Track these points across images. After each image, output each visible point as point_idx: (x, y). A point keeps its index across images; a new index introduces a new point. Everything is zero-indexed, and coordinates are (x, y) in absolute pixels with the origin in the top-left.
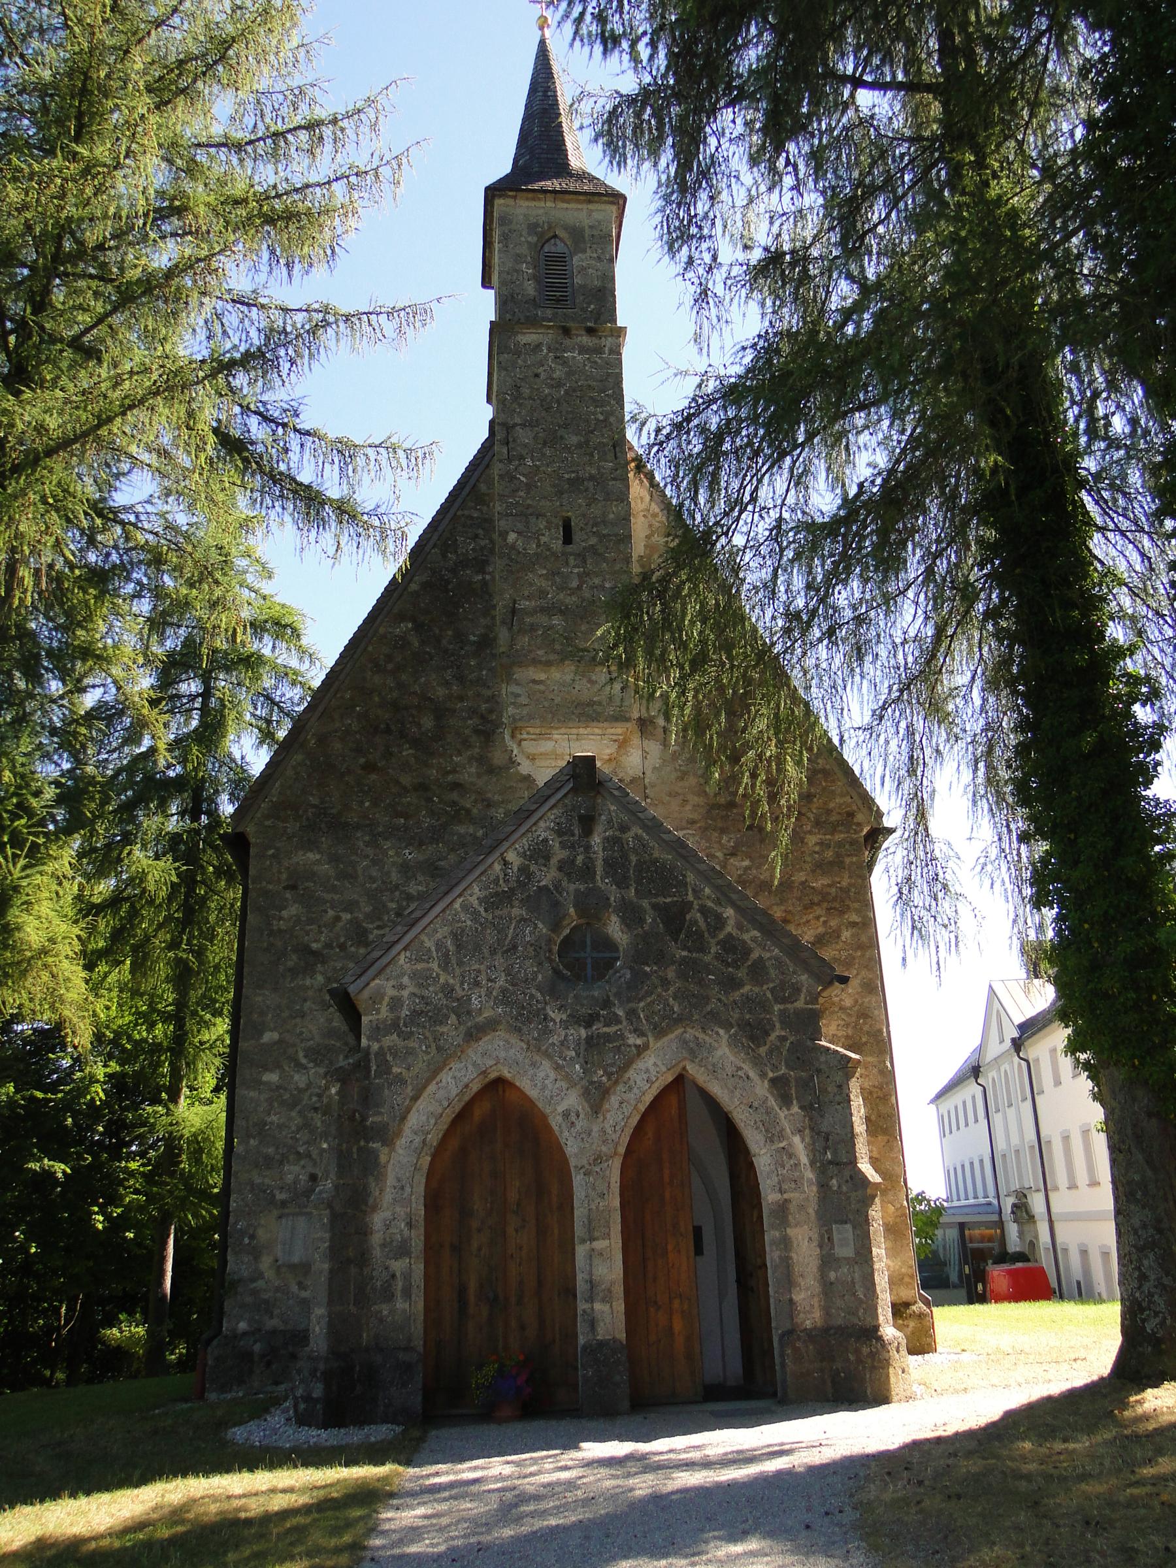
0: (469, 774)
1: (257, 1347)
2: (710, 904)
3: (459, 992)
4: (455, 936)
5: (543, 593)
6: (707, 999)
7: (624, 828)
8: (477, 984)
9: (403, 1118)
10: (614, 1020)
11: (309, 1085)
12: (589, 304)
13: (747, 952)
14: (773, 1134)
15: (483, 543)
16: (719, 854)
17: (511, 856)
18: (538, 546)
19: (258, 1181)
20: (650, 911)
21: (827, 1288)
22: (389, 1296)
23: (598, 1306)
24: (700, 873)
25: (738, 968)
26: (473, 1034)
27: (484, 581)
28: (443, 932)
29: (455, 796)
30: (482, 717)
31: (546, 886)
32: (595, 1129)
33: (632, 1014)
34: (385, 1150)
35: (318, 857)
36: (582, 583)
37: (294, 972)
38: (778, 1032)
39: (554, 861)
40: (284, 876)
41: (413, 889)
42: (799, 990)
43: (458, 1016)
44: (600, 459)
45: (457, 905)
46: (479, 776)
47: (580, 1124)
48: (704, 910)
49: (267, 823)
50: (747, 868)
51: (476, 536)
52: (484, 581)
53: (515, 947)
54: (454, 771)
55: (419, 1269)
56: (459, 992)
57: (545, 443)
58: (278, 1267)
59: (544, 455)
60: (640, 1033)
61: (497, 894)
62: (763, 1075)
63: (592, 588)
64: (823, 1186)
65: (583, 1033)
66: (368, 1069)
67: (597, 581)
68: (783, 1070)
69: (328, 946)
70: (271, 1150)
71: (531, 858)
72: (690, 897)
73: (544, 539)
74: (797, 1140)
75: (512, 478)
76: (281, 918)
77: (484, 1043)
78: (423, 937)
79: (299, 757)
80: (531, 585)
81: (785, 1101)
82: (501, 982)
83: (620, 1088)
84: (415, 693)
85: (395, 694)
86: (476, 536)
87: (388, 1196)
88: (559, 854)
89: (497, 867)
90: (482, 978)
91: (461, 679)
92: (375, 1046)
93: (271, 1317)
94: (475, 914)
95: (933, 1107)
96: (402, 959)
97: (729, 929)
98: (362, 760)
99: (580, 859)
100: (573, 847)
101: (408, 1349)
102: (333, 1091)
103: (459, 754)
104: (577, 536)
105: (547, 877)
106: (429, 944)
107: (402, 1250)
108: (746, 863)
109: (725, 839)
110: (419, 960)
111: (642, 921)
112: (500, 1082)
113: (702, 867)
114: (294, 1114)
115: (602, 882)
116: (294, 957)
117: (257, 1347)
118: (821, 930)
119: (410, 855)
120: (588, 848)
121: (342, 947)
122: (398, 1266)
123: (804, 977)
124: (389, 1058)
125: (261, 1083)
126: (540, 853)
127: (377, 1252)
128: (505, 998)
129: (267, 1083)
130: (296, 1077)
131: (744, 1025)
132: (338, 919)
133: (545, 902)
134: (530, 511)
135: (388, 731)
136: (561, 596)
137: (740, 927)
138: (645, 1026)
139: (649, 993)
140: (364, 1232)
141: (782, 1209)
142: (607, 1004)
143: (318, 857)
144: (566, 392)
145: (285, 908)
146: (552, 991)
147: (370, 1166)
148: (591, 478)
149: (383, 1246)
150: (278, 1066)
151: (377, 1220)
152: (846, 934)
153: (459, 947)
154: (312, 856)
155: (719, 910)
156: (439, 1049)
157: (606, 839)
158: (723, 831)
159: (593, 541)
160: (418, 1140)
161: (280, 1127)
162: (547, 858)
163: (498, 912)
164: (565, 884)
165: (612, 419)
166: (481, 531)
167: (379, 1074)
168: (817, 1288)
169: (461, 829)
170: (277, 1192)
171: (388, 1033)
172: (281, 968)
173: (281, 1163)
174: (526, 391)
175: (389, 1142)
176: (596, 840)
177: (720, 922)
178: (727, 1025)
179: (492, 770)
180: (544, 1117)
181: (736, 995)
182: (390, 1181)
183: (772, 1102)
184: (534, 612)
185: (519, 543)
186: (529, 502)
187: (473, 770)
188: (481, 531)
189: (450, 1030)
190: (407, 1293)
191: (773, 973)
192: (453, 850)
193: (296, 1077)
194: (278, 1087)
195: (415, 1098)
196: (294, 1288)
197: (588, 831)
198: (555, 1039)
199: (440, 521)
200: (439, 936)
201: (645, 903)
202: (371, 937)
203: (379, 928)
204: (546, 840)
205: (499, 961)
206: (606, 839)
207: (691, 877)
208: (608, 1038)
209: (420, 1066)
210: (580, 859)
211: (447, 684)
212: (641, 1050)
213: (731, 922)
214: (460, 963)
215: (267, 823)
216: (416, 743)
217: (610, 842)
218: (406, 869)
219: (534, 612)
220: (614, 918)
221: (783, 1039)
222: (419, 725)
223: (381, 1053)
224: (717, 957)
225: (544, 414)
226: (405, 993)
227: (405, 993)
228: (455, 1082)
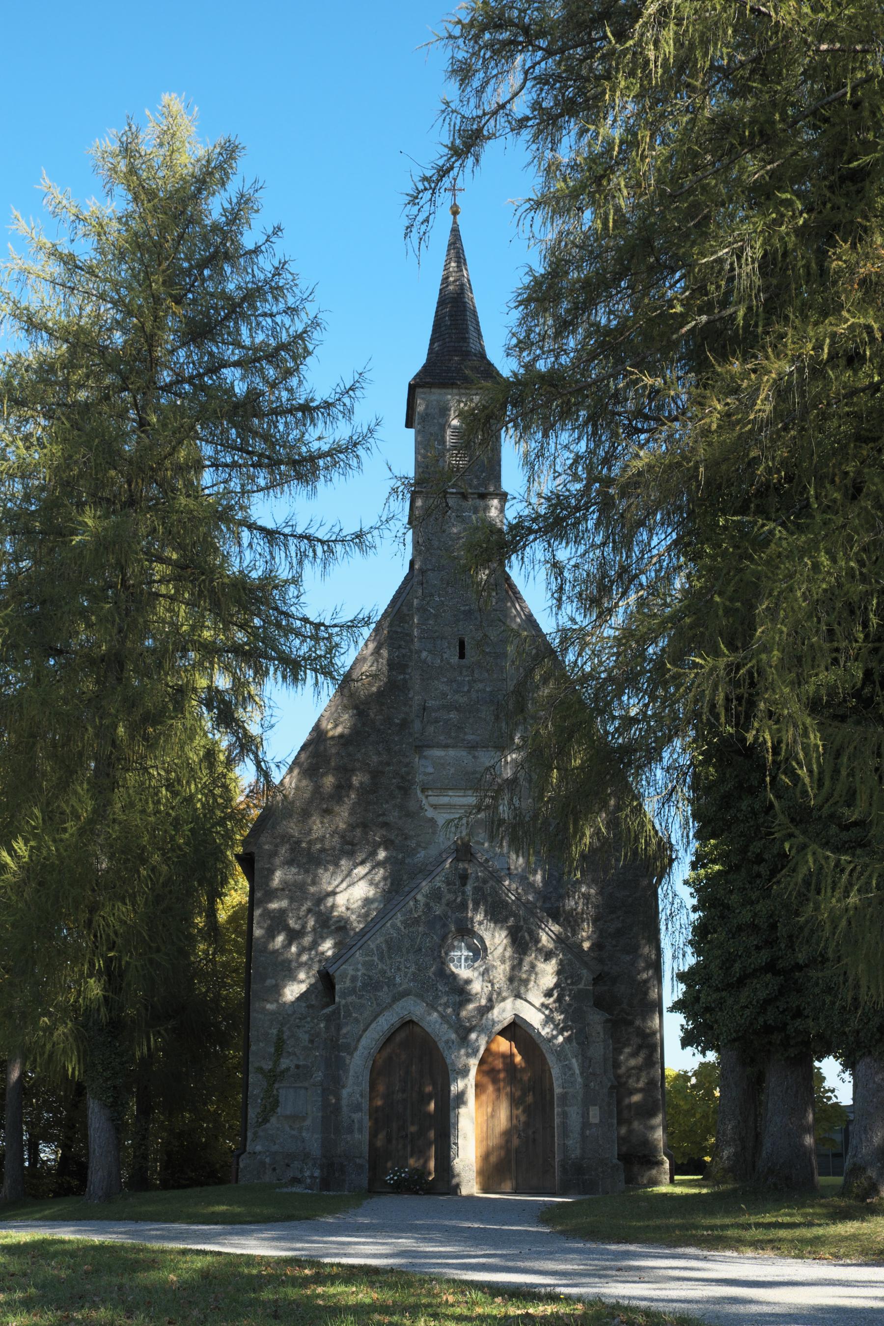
1: (268, 1160)
3: (389, 974)
5: (444, 695)
7: (485, 882)
8: (399, 969)
9: (359, 1040)
15: (404, 651)
17: (419, 897)
18: (442, 661)
21: (584, 1137)
22: (350, 1131)
26: (397, 998)
27: (404, 679)
28: (380, 940)
30: (402, 777)
34: (348, 1057)
39: (444, 901)
42: (581, 979)
45: (388, 925)
46: (400, 818)
51: (400, 647)
52: (404, 679)
53: (420, 949)
54: (384, 814)
56: (389, 974)
63: (477, 691)
64: (586, 1086)
66: (339, 1013)
67: (480, 686)
72: (522, 923)
74: (574, 1061)
77: (401, 1003)
78: (369, 942)
86: (400, 647)
87: (351, 1081)
89: (411, 903)
90: (402, 967)
92: (343, 1002)
99: (459, 900)
102: (322, 1025)
103: (387, 802)
106: (372, 946)
107: (357, 1108)
112: (411, 1022)
120: (464, 893)
122: (356, 1116)
123: (585, 971)
136: (456, 697)
149: (348, 1106)
153: (389, 948)
156: (378, 1005)
157: (475, 888)
160: (366, 1052)
162: (440, 899)
166: (403, 643)
167: (345, 1017)
174: (436, 543)
175: (351, 1054)
179: (409, 815)
180: (435, 1042)
182: (351, 1073)
187: (396, 814)
188: (403, 643)
189: (384, 995)
190: (360, 1130)
195: (365, 1030)
197: (464, 884)
206: (475, 888)
210: (459, 900)
226: (359, 973)
228: (386, 1022)
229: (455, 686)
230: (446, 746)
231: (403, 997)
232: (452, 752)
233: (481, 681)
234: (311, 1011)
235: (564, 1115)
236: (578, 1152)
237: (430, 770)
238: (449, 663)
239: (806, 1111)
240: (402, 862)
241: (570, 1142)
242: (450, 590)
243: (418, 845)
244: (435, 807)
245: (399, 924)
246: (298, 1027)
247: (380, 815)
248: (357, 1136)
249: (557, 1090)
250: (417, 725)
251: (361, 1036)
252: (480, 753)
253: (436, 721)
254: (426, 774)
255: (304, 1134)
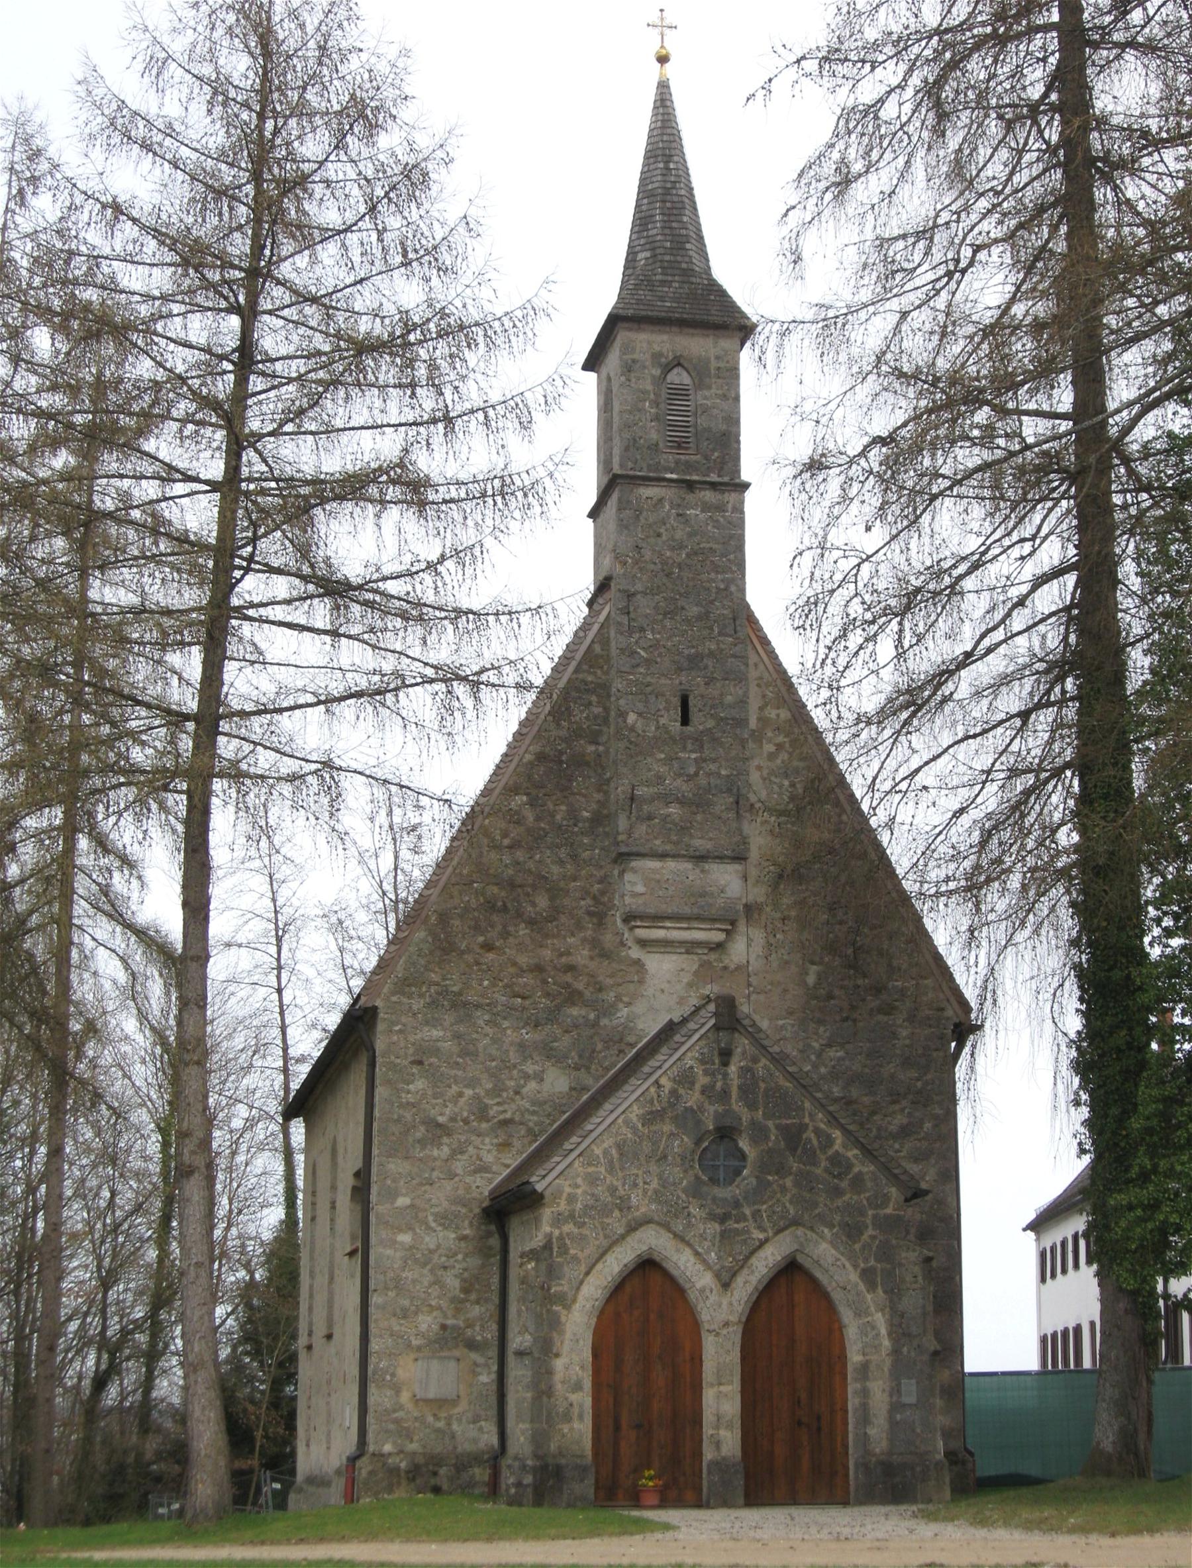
1: (403, 1465)
2: (822, 1126)
4: (618, 1146)
5: (660, 779)
6: (816, 1205)
7: (755, 1060)
8: (635, 1185)
9: (578, 1289)
10: (742, 1218)
11: (439, 1246)
12: (713, 450)
13: (850, 1166)
16: (816, 1045)
17: (663, 1081)
18: (658, 728)
19: (396, 1328)
20: (774, 1130)
21: (893, 1424)
23: (722, 1432)
25: (841, 1179)
26: (632, 1228)
28: (608, 1142)
29: (568, 978)
31: (691, 1108)
32: (725, 1302)
33: (756, 1214)
34: (564, 1312)
35: (441, 1034)
36: (699, 768)
37: (423, 1143)
38: (870, 1231)
39: (698, 1087)
40: (411, 1051)
41: (530, 1068)
42: (889, 1199)
43: (621, 1210)
44: (720, 634)
45: (620, 1121)
46: (592, 958)
47: (713, 1298)
48: (817, 1131)
49: (394, 999)
50: (840, 1059)
53: (665, 1157)
54: (569, 954)
55: (588, 1401)
57: (665, 614)
58: (416, 1400)
59: (664, 627)
60: (762, 1229)
61: (652, 1112)
62: (855, 1266)
63: (708, 775)
64: (896, 1351)
65: (717, 1226)
67: (713, 767)
68: (872, 1262)
69: (453, 1119)
70: (406, 1303)
71: (680, 1083)
72: (807, 1120)
73: (662, 721)
75: (633, 653)
76: (409, 1092)
77: (638, 1234)
79: (421, 934)
80: (650, 770)
81: (872, 1286)
82: (655, 1184)
83: (745, 1271)
84: (529, 871)
85: (511, 872)
86: (590, 703)
88: (702, 1080)
89: (653, 1090)
90: (640, 1181)
91: (574, 857)
93: (412, 1441)
94: (634, 1130)
95: (1031, 1235)
97: (836, 1147)
98: (481, 939)
100: (713, 1074)
101: (582, 1457)
103: (573, 935)
104: (695, 716)
105: (692, 1099)
106: (598, 1151)
107: (578, 1387)
108: (841, 1054)
109: (822, 1029)
110: (590, 1164)
111: (767, 1138)
114: (425, 1271)
115: (737, 1106)
116: (422, 1129)
117: (403, 1465)
118: (905, 1121)
119: (527, 1035)
120: (725, 1075)
121: (466, 1121)
122: (574, 1397)
123: (893, 1190)
124: (568, 1242)
125: (395, 1242)
126: (685, 1079)
127: (559, 1386)
128: (657, 1197)
129: (402, 1243)
130: (427, 1239)
131: (845, 1226)
132: (461, 1094)
133: (688, 1119)
134: (649, 689)
135: (505, 909)
137: (844, 1146)
138: (767, 1224)
139: (771, 1198)
140: (550, 1372)
141: (864, 1370)
142: (737, 1204)
143: (441, 1034)
144: (688, 555)
145: (412, 1082)
146: (695, 1191)
147: (555, 1324)
148: (711, 654)
150: (410, 1228)
151: (559, 1364)
152: (928, 1126)
154: (436, 1033)
155: (830, 1131)
156: (606, 1237)
158: (820, 1022)
159: (710, 723)
161: (414, 1281)
162: (693, 1083)
163: (653, 1128)
164: (706, 1105)
165: (733, 588)
166: (594, 698)
168: (886, 1427)
169: (575, 1011)
170: (412, 1338)
171: (566, 1222)
172: (411, 1140)
173: (416, 1313)
175: (568, 1308)
176: (733, 1069)
178: (831, 1226)
181: (839, 1202)
183: (862, 1287)
184: (652, 800)
185: (639, 724)
186: (649, 679)
187: (585, 952)
190: (581, 1417)
191: (869, 1184)
192: (566, 1032)
193: (427, 1239)
194: (411, 1248)
195: (587, 1273)
196: (430, 1419)
197: (726, 1064)
200: (605, 1145)
201: (770, 1124)
202: (492, 1113)
203: (498, 1104)
204: (692, 1067)
205: (653, 1168)
208: (737, 1232)
209: (590, 1250)
210: (719, 1085)
211: (561, 863)
212: (762, 1244)
213: (839, 1141)
214: (622, 1169)
215: (394, 999)
216: (531, 922)
217: (744, 1071)
218: (522, 1046)
219: (652, 800)
221: (873, 1237)
222: (534, 904)
223: (561, 1238)
224: (826, 1170)
225: (665, 580)
227: (579, 1191)
229: (676, 765)
230: (663, 856)
231: (641, 1225)
232: (671, 864)
233: (714, 761)
234: (463, 1244)
235: (865, 1393)
236: (884, 1444)
237: (640, 889)
238: (667, 732)
240: (595, 1024)
241: (872, 1431)
242: (668, 623)
243: (618, 998)
244: (643, 943)
245: (635, 1119)
246: (445, 1268)
247: (561, 955)
248: (576, 1425)
250: (622, 823)
251: (581, 1283)
253: (650, 818)
254: (635, 895)
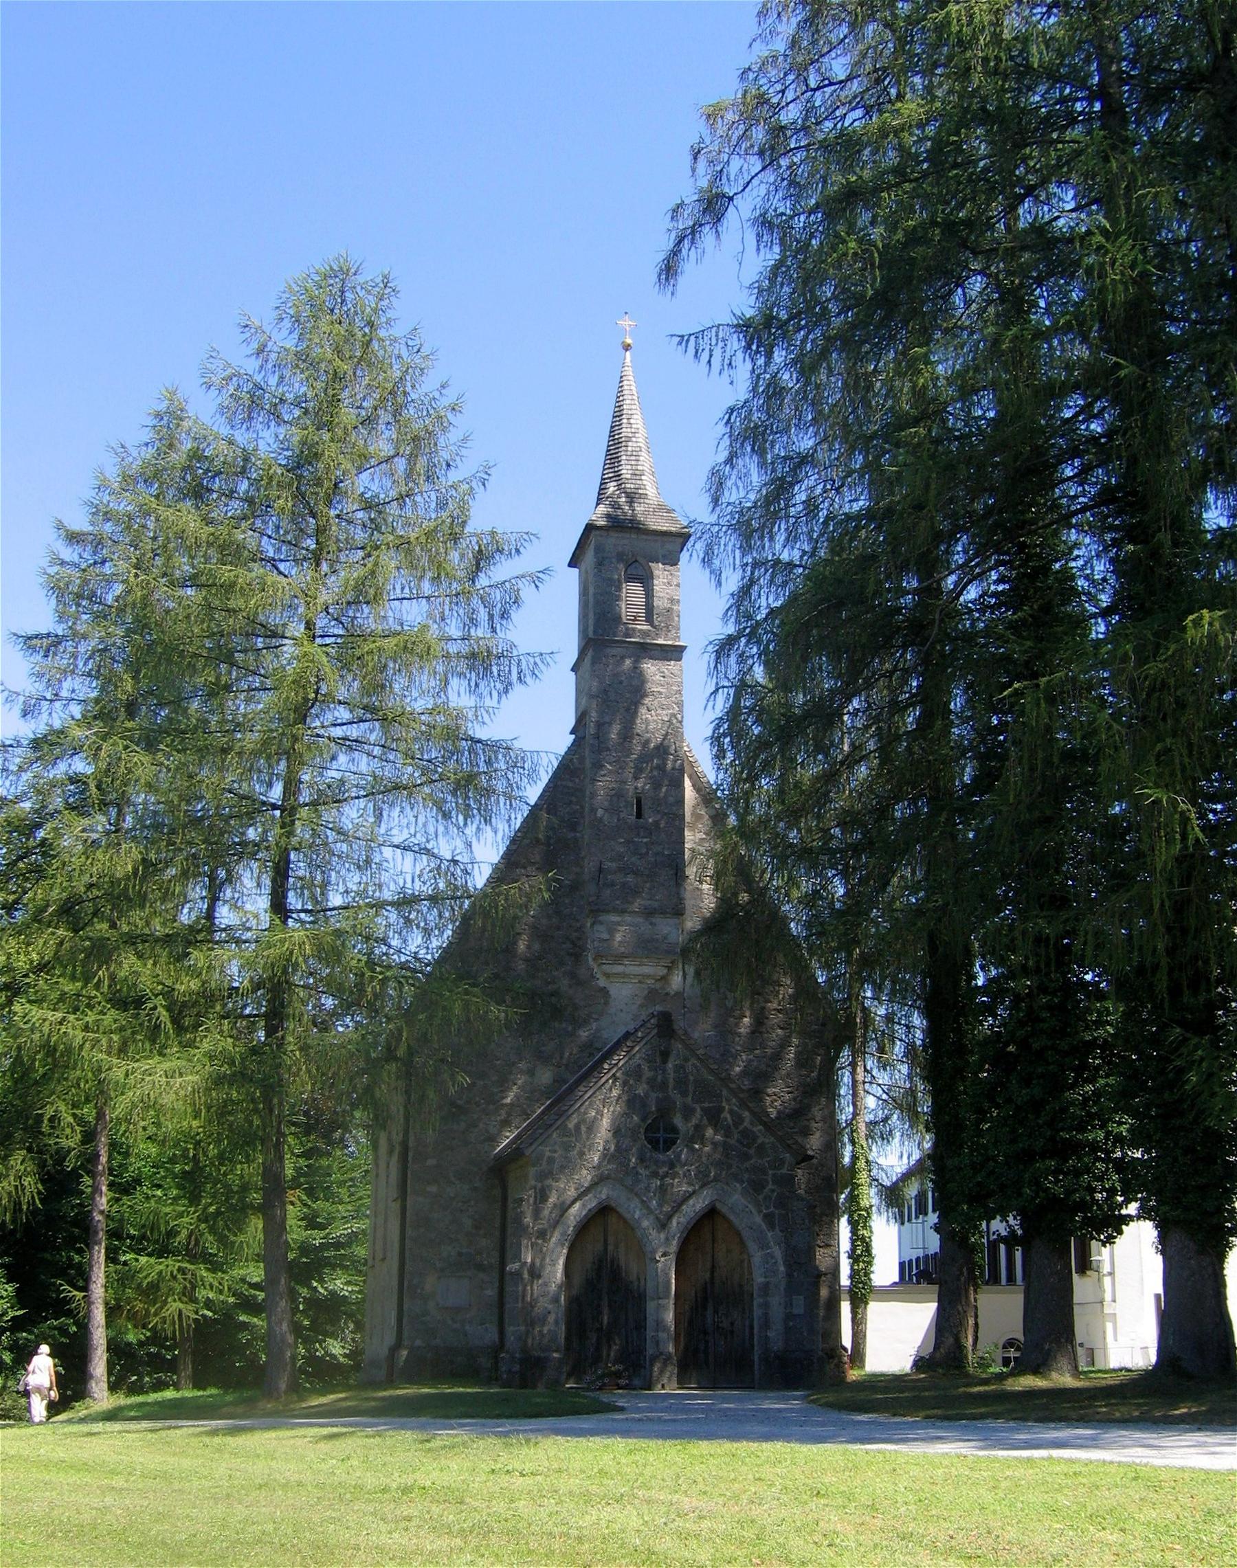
0: (564, 984)
7: (686, 1060)
13: (755, 1138)
14: (763, 1246)
24: (731, 1090)
38: (770, 1186)
39: (644, 1079)
46: (570, 986)
62: (760, 1212)
64: (789, 1275)
67: (659, 849)
68: (772, 1209)
73: (622, 815)
81: (771, 1226)
88: (648, 1074)
96: (555, 1135)
104: (646, 811)
113: (733, 1086)
115: (674, 1094)
120: (664, 1071)
136: (633, 859)
162: (640, 1077)
177: (741, 1120)
181: (747, 1164)
188: (574, 799)
196: (450, 1322)
197: (665, 1062)
198: (642, 1186)
199: (886, 1389)
204: (639, 1065)
207: (725, 1092)
217: (679, 1068)
220: (678, 1115)
221: (773, 1191)
224: (738, 1141)
235: (766, 1305)
239: (967, 1291)
244: (607, 975)
249: (759, 1279)
252: (658, 920)
253: (613, 884)
255: (467, 1327)
